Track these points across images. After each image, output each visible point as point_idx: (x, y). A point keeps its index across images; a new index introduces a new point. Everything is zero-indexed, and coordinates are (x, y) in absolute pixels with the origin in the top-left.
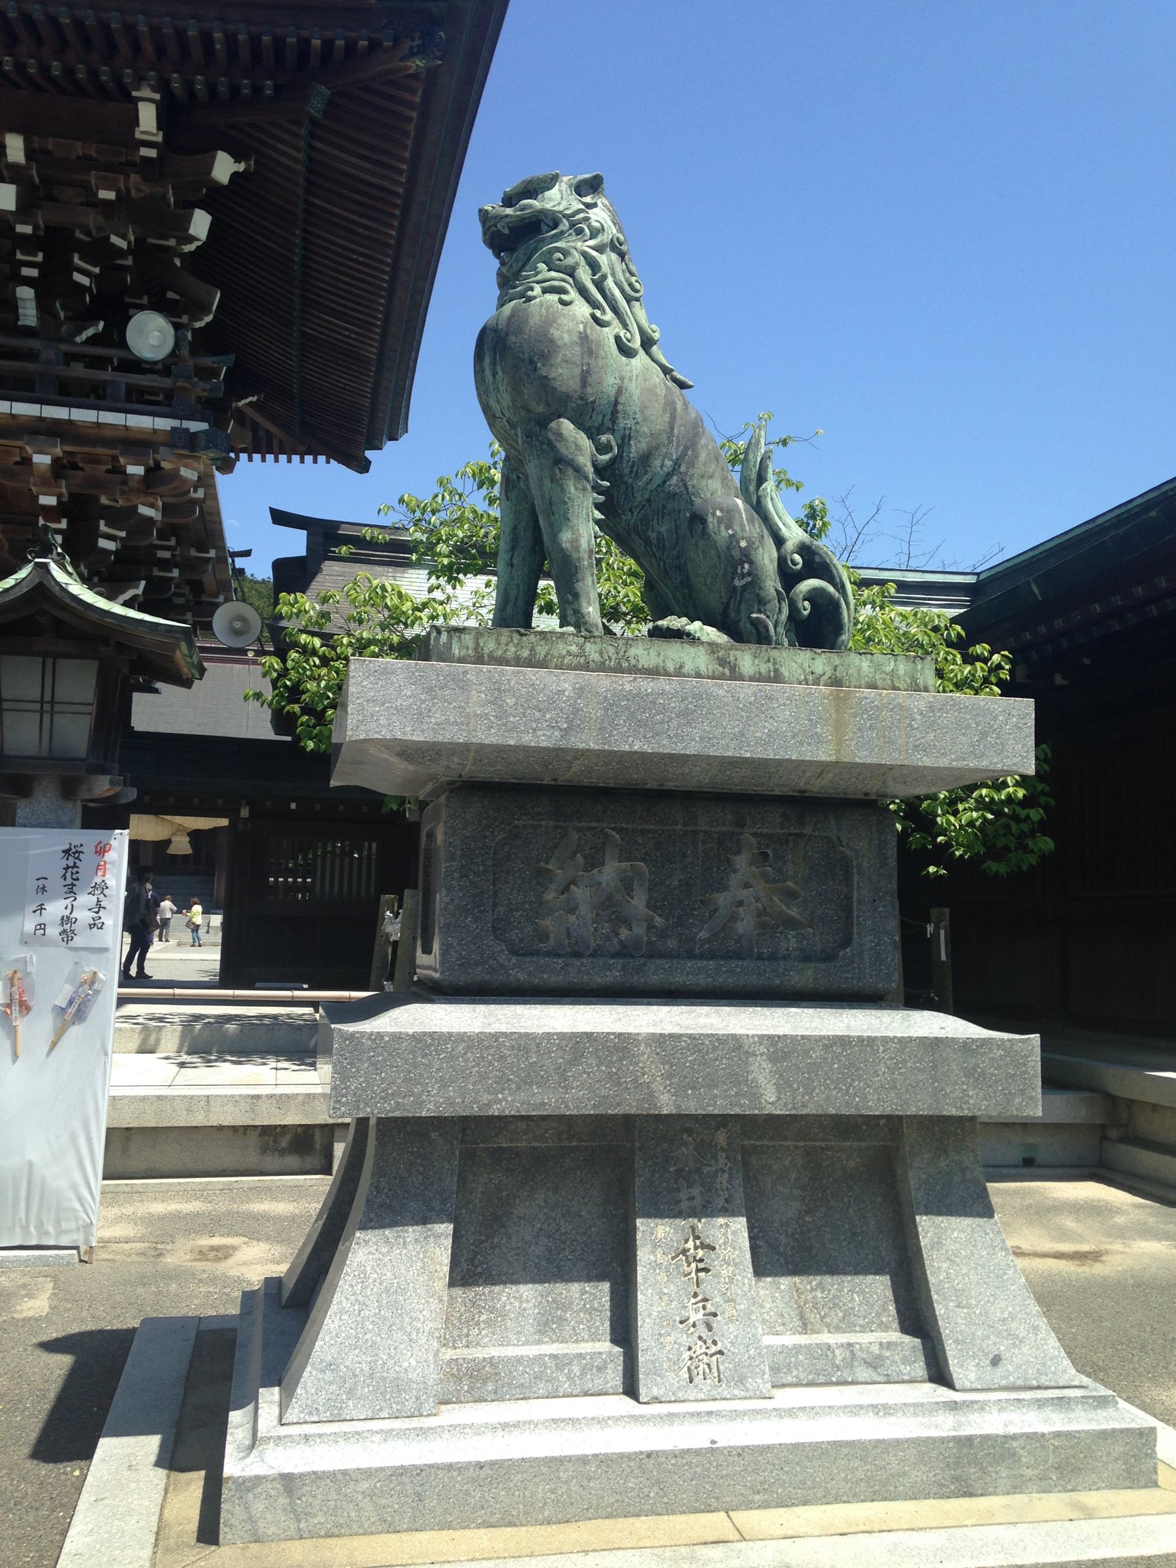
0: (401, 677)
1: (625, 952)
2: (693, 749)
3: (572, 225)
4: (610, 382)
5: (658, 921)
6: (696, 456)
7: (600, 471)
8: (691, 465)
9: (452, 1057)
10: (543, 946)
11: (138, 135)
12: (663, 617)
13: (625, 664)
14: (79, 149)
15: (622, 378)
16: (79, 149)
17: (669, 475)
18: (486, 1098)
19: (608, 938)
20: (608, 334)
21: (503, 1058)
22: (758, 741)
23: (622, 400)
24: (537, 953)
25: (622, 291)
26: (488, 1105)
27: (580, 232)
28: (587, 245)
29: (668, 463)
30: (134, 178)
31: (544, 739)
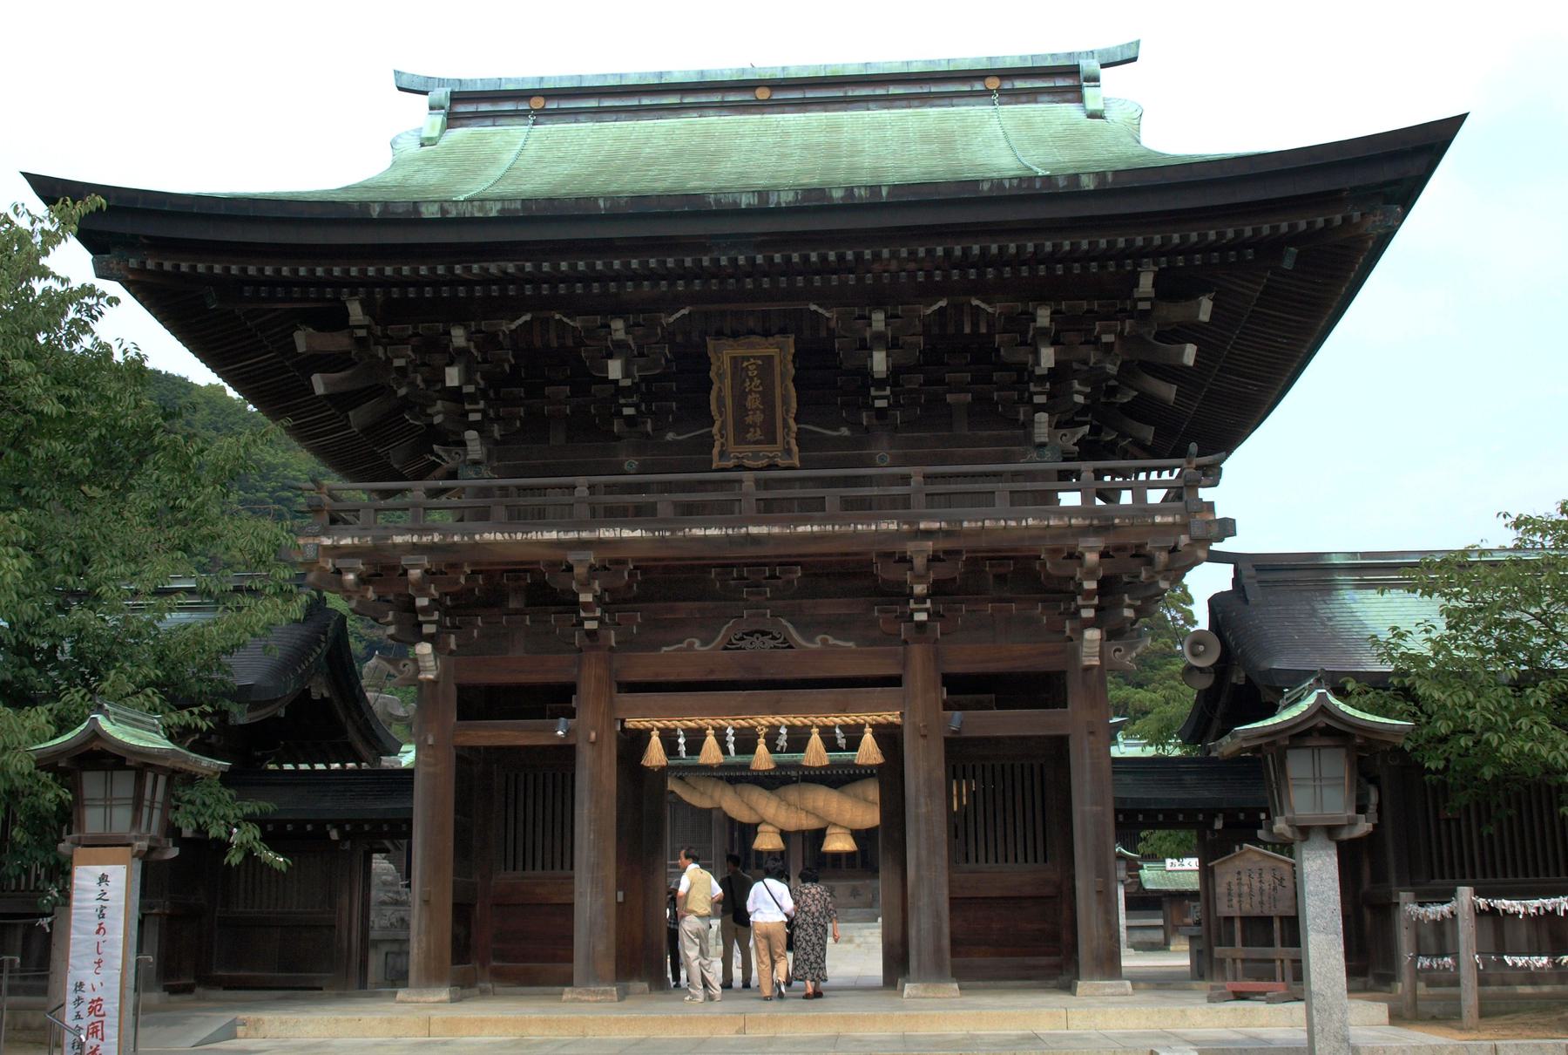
16: (1085, 305)
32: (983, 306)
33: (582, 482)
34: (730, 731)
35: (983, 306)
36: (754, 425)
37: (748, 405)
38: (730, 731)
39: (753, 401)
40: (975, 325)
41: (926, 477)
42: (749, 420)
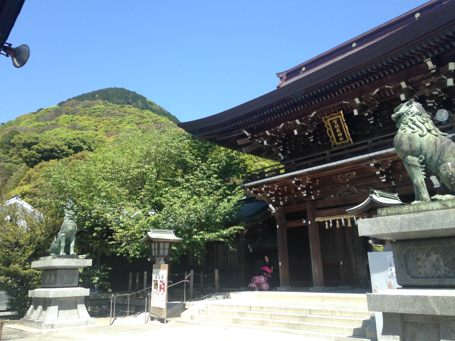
0: (366, 222)
1: (439, 277)
2: (430, 228)
3: (407, 113)
4: (418, 145)
5: (448, 269)
6: (444, 153)
7: (422, 164)
8: (443, 156)
9: (389, 300)
10: (419, 276)
11: (430, 69)
12: (433, 196)
13: (419, 210)
14: (419, 77)
15: (421, 142)
16: (419, 77)
17: (438, 160)
18: (397, 309)
19: (435, 273)
20: (417, 135)
21: (399, 301)
22: (447, 224)
23: (422, 147)
24: (418, 278)
25: (421, 122)
26: (398, 310)
27: (408, 114)
28: (410, 117)
29: (437, 157)
30: (433, 78)
31: (396, 231)
32: (389, 87)
33: (370, 141)
34: (331, 221)
35: (389, 87)
36: (340, 136)
37: (338, 132)
38: (343, 220)
39: (338, 130)
40: (390, 93)
41: (296, 162)
42: (339, 135)
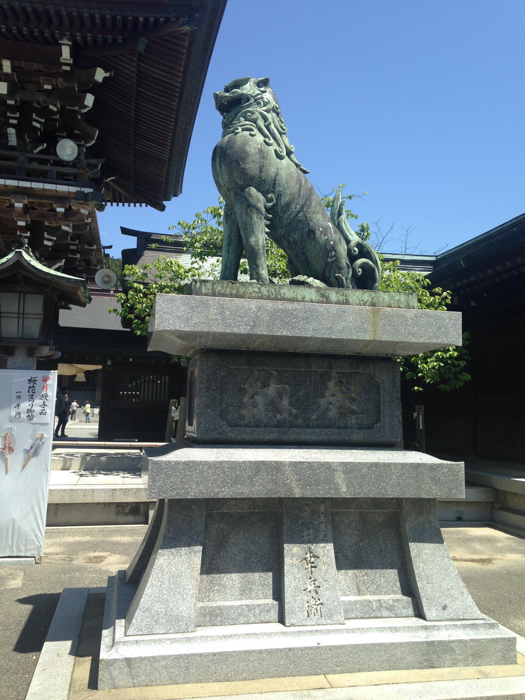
0: (179, 302)
1: (279, 425)
2: (309, 334)
3: (255, 100)
4: (272, 171)
5: (294, 411)
6: (311, 204)
7: (268, 210)
8: (309, 207)
9: (202, 472)
10: (242, 423)
11: (62, 60)
12: (296, 276)
13: (279, 297)
14: (35, 66)
15: (278, 169)
16: (35, 66)
17: (299, 212)
18: (217, 490)
19: (271, 419)
20: (272, 149)
21: (225, 472)
22: (339, 331)
23: (278, 178)
24: (240, 426)
25: (278, 130)
26: (218, 493)
27: (259, 103)
28: (262, 110)
29: (298, 207)
30: (60, 80)
31: (243, 330)
